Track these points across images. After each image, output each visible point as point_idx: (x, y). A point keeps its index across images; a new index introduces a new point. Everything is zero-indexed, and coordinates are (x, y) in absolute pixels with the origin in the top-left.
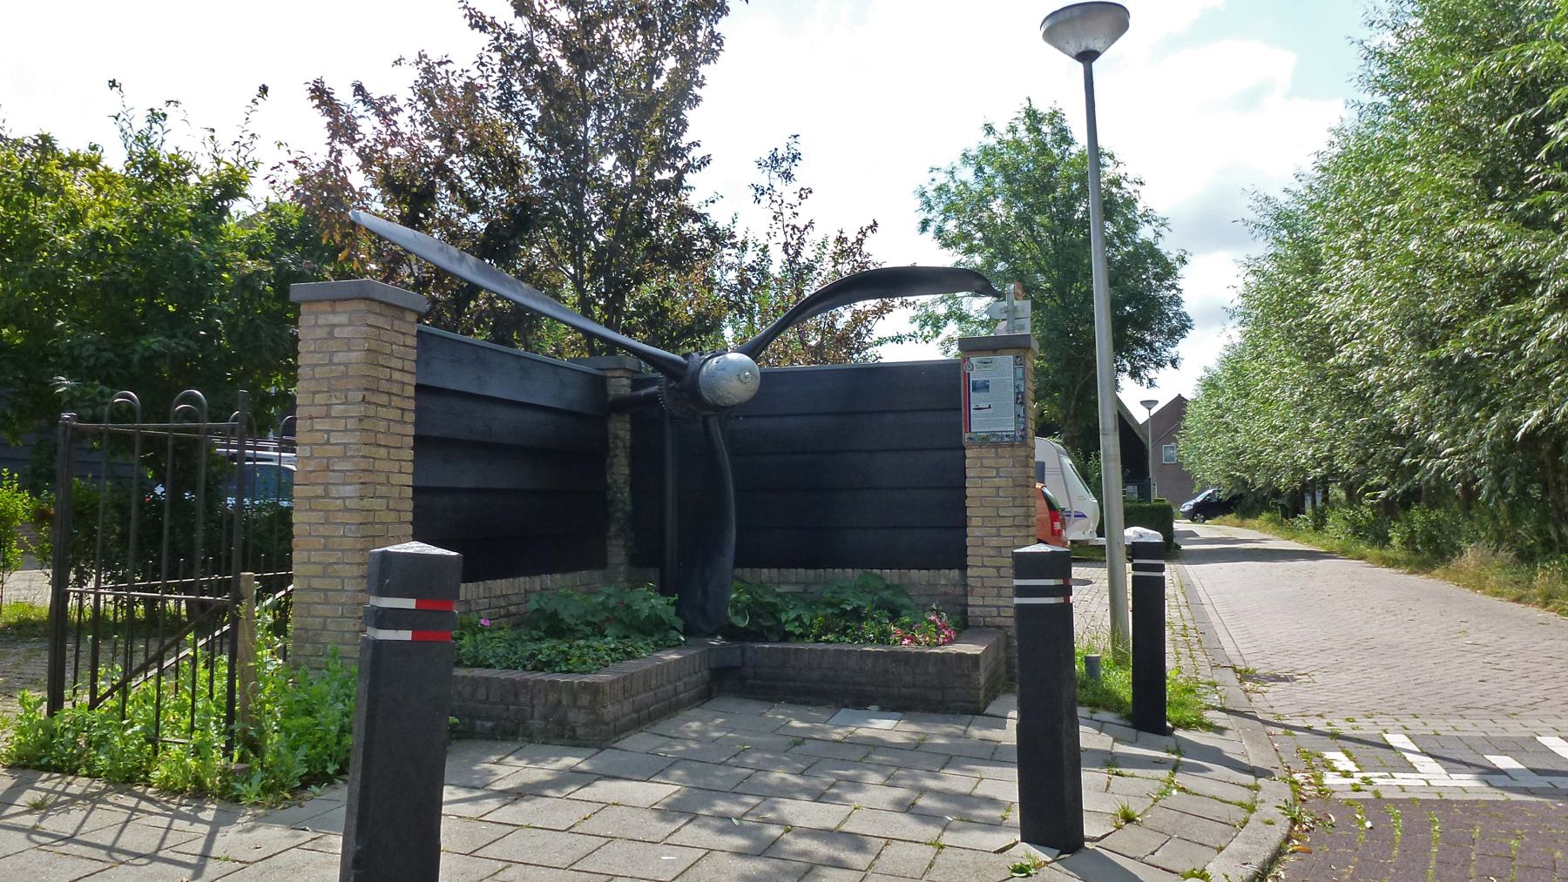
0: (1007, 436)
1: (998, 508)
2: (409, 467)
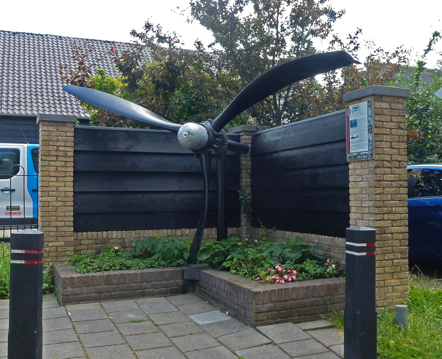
0: (365, 154)
1: (362, 201)
2: (71, 184)
